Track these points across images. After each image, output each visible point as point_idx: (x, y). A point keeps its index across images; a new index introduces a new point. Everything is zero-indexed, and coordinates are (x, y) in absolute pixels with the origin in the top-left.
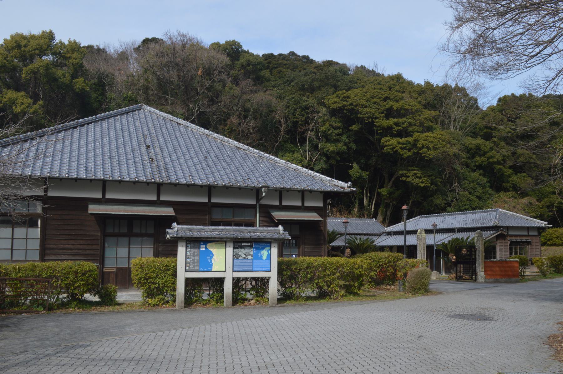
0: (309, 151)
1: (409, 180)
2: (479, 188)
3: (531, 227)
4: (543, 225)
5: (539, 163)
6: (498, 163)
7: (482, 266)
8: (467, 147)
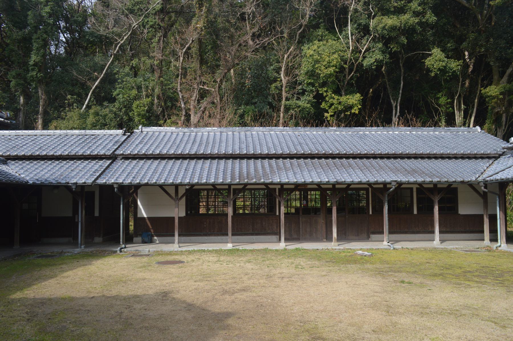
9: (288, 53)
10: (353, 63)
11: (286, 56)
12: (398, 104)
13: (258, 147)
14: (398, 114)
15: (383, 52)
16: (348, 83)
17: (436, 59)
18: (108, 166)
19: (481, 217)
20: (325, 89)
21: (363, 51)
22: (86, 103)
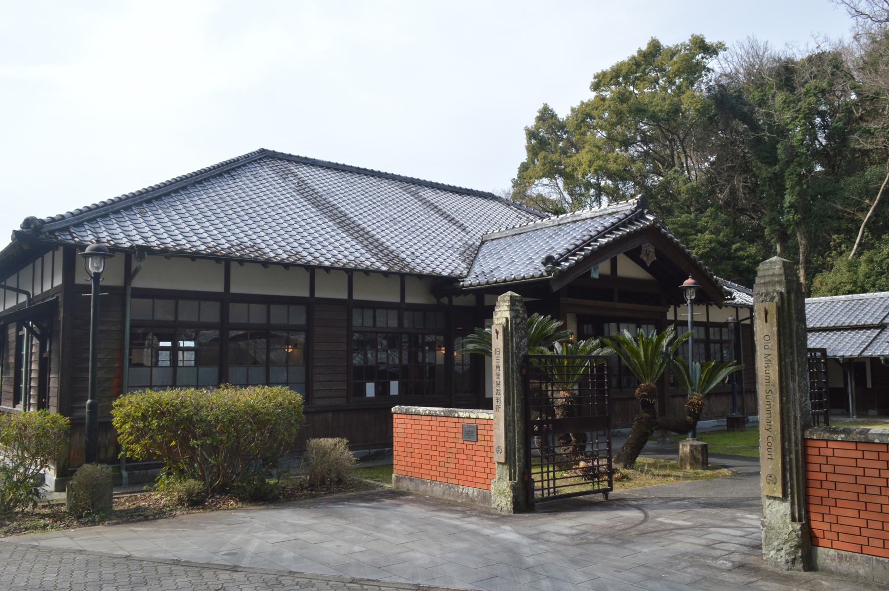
18: (878, 335)
22: (857, 241)
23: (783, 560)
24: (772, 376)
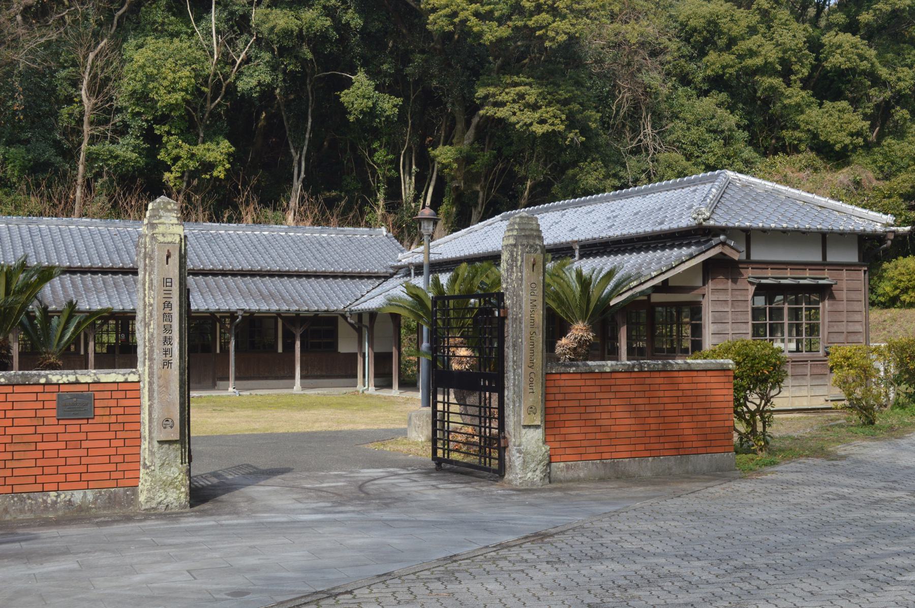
0: (218, 32)
1: (502, 113)
2: (714, 144)
3: (832, 232)
4: (879, 228)
5: (883, 72)
6: (766, 69)
7: (535, 398)
8: (683, 25)
9: (96, 51)
10: (219, 79)
11: (91, 56)
12: (303, 159)
13: (54, 255)
14: (303, 175)
15: (274, 68)
16: (211, 113)
17: (359, 92)
19: (355, 355)
20: (166, 128)
21: (238, 62)
23: (538, 478)
24: (536, 320)
